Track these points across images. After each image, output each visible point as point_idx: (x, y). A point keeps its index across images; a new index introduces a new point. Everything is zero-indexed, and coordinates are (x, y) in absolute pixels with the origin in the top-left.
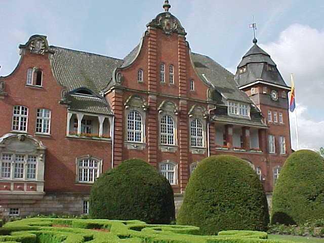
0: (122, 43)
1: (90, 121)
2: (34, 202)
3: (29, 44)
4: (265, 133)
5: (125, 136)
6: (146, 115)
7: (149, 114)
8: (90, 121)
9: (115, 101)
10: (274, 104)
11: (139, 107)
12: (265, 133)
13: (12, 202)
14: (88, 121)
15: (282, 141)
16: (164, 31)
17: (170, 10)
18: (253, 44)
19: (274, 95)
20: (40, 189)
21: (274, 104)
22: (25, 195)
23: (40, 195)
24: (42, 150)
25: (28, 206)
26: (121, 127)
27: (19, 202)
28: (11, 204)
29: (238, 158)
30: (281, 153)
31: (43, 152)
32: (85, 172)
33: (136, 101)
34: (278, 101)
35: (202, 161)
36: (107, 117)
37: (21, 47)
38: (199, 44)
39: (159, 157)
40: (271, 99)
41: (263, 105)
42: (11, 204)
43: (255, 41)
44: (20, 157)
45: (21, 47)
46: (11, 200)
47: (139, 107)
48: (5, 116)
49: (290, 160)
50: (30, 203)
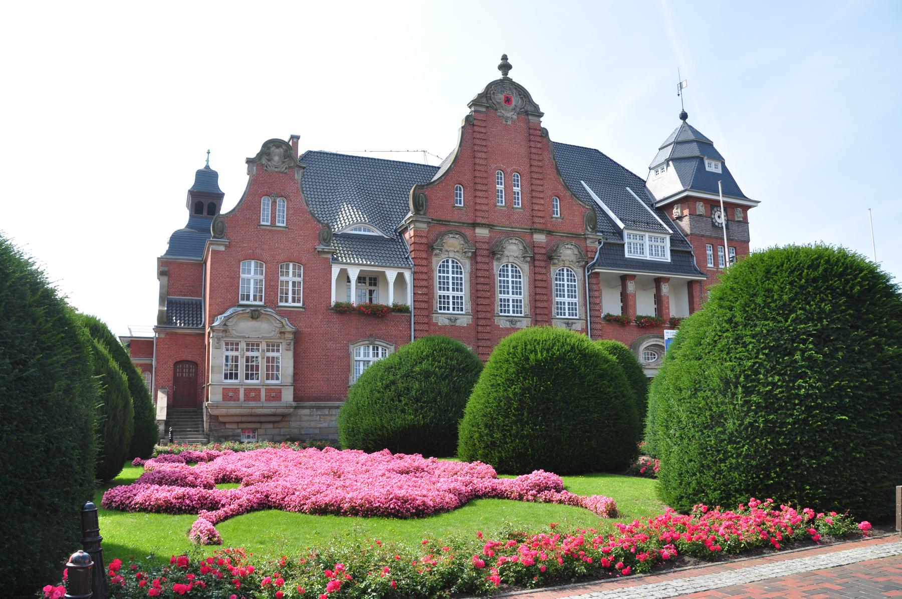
0: (433, 141)
1: (375, 279)
2: (279, 418)
3: (260, 155)
5: (434, 302)
6: (471, 264)
8: (375, 279)
9: (414, 243)
13: (244, 419)
14: (370, 279)
16: (295, 138)
17: (511, 74)
18: (682, 121)
20: (288, 396)
22: (262, 407)
23: (287, 407)
24: (289, 332)
25: (271, 426)
27: (254, 419)
28: (242, 422)
31: (291, 336)
35: (403, 349)
36: (401, 271)
40: (713, 224)
42: (242, 422)
43: (684, 116)
44: (273, 346)
45: (249, 161)
46: (242, 416)
48: (228, 280)
49: (514, 343)
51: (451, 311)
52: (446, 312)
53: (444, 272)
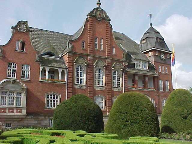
0: (72, 26)
1: (54, 72)
2: (20, 120)
3: (17, 26)
4: (157, 79)
5: (74, 81)
6: (87, 68)
7: (88, 68)
8: (54, 72)
9: (68, 60)
10: (162, 62)
11: (82, 64)
12: (157, 79)
13: (7, 120)
14: (52, 72)
15: (167, 84)
17: (101, 6)
18: (150, 26)
19: (163, 56)
20: (24, 112)
21: (162, 62)
22: (15, 115)
23: (24, 116)
24: (25, 89)
25: (17, 122)
26: (71, 75)
27: (11, 120)
28: (6, 121)
29: (141, 94)
30: (166, 91)
31: (26, 90)
32: (50, 102)
33: (81, 60)
34: (165, 60)
35: (120, 96)
36: (63, 69)
37: (12, 28)
38: (118, 26)
39: (94, 93)
40: (161, 59)
41: (156, 62)
42: (6, 121)
43: (151, 25)
44: (12, 93)
45: (12, 28)
46: (6, 118)
47: (82, 64)
48: (3, 69)
49: (172, 95)
50: (18, 120)
51: (117, 87)
52: (98, 85)
53: (77, 72)
